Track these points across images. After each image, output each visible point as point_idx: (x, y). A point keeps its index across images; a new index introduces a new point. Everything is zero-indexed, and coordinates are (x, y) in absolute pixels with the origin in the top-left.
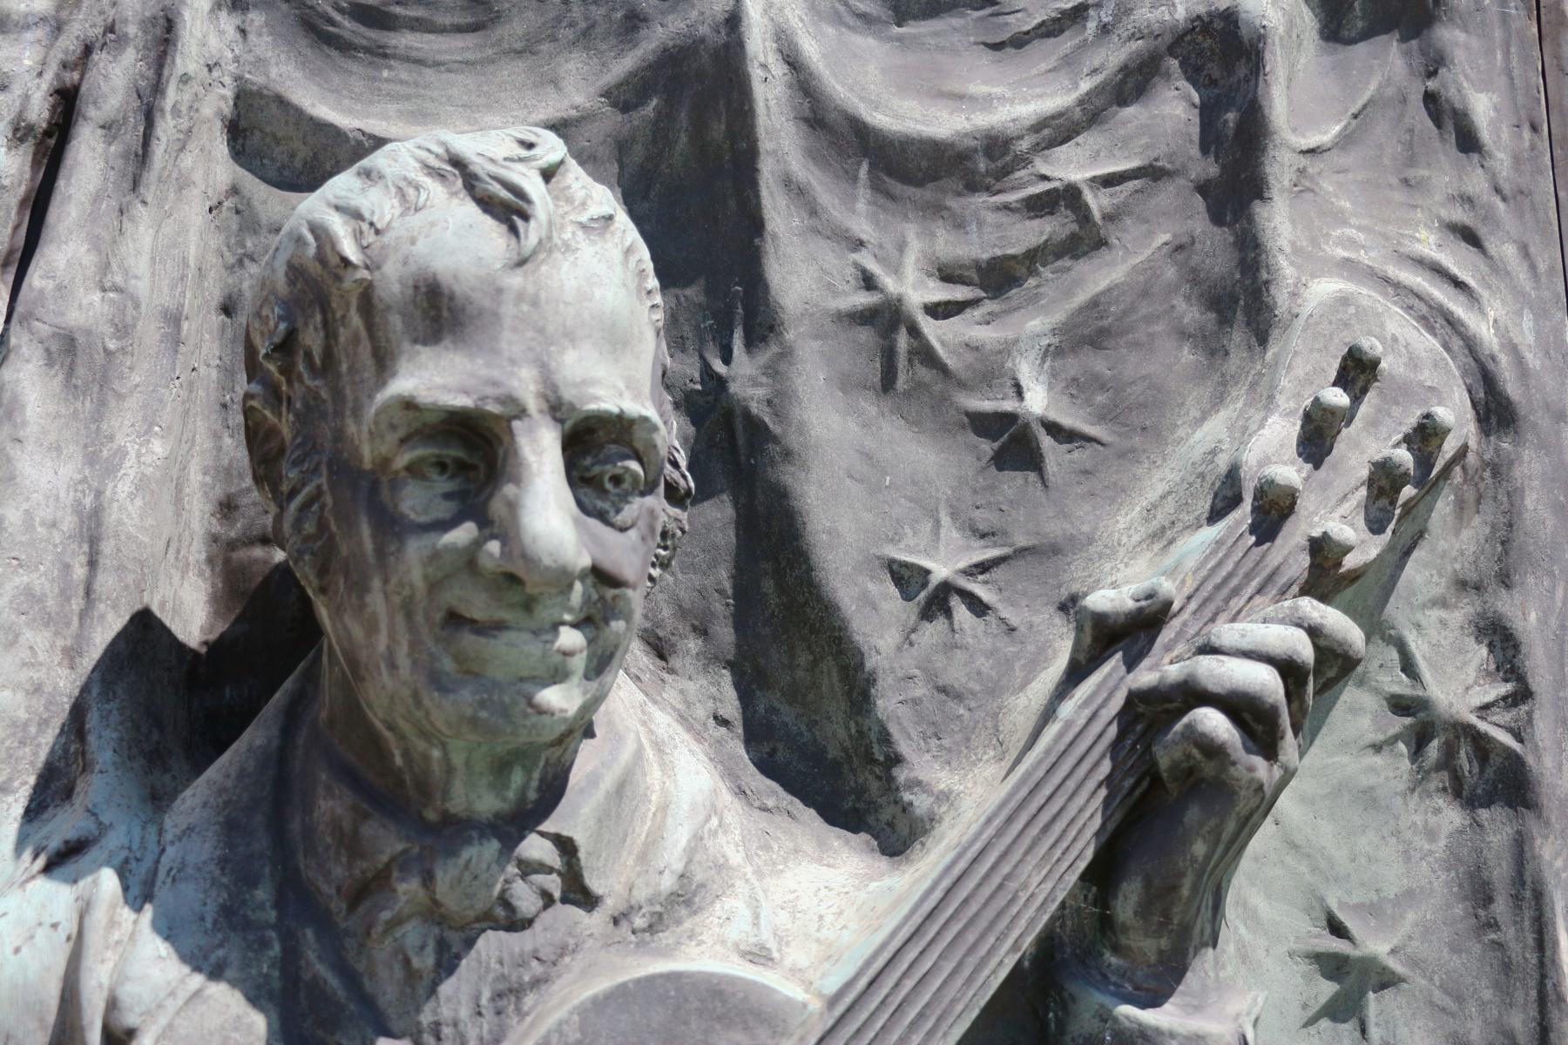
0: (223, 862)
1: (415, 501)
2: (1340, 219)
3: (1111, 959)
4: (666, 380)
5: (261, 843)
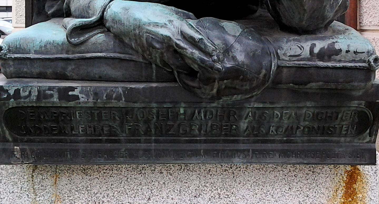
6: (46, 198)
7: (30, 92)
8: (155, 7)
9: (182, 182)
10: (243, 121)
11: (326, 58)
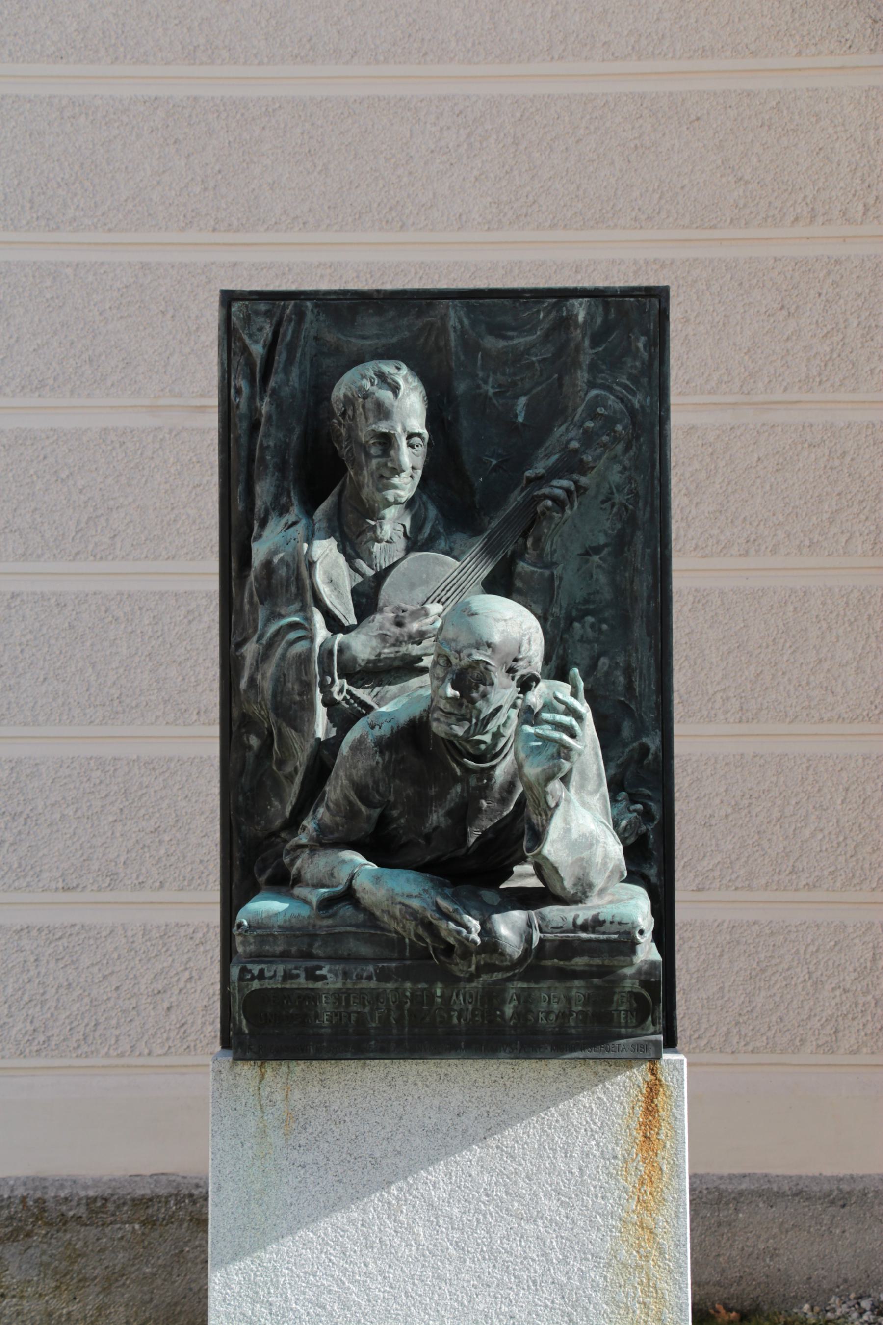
0: (328, 527)
1: (374, 451)
2: (602, 372)
3: (527, 556)
4: (586, 920)
5: (336, 523)
6: (276, 1116)
7: (275, 971)
8: (408, 875)
9: (441, 1096)
10: (508, 1005)
11: (590, 929)
